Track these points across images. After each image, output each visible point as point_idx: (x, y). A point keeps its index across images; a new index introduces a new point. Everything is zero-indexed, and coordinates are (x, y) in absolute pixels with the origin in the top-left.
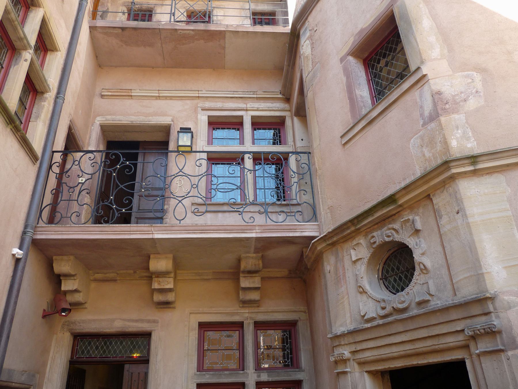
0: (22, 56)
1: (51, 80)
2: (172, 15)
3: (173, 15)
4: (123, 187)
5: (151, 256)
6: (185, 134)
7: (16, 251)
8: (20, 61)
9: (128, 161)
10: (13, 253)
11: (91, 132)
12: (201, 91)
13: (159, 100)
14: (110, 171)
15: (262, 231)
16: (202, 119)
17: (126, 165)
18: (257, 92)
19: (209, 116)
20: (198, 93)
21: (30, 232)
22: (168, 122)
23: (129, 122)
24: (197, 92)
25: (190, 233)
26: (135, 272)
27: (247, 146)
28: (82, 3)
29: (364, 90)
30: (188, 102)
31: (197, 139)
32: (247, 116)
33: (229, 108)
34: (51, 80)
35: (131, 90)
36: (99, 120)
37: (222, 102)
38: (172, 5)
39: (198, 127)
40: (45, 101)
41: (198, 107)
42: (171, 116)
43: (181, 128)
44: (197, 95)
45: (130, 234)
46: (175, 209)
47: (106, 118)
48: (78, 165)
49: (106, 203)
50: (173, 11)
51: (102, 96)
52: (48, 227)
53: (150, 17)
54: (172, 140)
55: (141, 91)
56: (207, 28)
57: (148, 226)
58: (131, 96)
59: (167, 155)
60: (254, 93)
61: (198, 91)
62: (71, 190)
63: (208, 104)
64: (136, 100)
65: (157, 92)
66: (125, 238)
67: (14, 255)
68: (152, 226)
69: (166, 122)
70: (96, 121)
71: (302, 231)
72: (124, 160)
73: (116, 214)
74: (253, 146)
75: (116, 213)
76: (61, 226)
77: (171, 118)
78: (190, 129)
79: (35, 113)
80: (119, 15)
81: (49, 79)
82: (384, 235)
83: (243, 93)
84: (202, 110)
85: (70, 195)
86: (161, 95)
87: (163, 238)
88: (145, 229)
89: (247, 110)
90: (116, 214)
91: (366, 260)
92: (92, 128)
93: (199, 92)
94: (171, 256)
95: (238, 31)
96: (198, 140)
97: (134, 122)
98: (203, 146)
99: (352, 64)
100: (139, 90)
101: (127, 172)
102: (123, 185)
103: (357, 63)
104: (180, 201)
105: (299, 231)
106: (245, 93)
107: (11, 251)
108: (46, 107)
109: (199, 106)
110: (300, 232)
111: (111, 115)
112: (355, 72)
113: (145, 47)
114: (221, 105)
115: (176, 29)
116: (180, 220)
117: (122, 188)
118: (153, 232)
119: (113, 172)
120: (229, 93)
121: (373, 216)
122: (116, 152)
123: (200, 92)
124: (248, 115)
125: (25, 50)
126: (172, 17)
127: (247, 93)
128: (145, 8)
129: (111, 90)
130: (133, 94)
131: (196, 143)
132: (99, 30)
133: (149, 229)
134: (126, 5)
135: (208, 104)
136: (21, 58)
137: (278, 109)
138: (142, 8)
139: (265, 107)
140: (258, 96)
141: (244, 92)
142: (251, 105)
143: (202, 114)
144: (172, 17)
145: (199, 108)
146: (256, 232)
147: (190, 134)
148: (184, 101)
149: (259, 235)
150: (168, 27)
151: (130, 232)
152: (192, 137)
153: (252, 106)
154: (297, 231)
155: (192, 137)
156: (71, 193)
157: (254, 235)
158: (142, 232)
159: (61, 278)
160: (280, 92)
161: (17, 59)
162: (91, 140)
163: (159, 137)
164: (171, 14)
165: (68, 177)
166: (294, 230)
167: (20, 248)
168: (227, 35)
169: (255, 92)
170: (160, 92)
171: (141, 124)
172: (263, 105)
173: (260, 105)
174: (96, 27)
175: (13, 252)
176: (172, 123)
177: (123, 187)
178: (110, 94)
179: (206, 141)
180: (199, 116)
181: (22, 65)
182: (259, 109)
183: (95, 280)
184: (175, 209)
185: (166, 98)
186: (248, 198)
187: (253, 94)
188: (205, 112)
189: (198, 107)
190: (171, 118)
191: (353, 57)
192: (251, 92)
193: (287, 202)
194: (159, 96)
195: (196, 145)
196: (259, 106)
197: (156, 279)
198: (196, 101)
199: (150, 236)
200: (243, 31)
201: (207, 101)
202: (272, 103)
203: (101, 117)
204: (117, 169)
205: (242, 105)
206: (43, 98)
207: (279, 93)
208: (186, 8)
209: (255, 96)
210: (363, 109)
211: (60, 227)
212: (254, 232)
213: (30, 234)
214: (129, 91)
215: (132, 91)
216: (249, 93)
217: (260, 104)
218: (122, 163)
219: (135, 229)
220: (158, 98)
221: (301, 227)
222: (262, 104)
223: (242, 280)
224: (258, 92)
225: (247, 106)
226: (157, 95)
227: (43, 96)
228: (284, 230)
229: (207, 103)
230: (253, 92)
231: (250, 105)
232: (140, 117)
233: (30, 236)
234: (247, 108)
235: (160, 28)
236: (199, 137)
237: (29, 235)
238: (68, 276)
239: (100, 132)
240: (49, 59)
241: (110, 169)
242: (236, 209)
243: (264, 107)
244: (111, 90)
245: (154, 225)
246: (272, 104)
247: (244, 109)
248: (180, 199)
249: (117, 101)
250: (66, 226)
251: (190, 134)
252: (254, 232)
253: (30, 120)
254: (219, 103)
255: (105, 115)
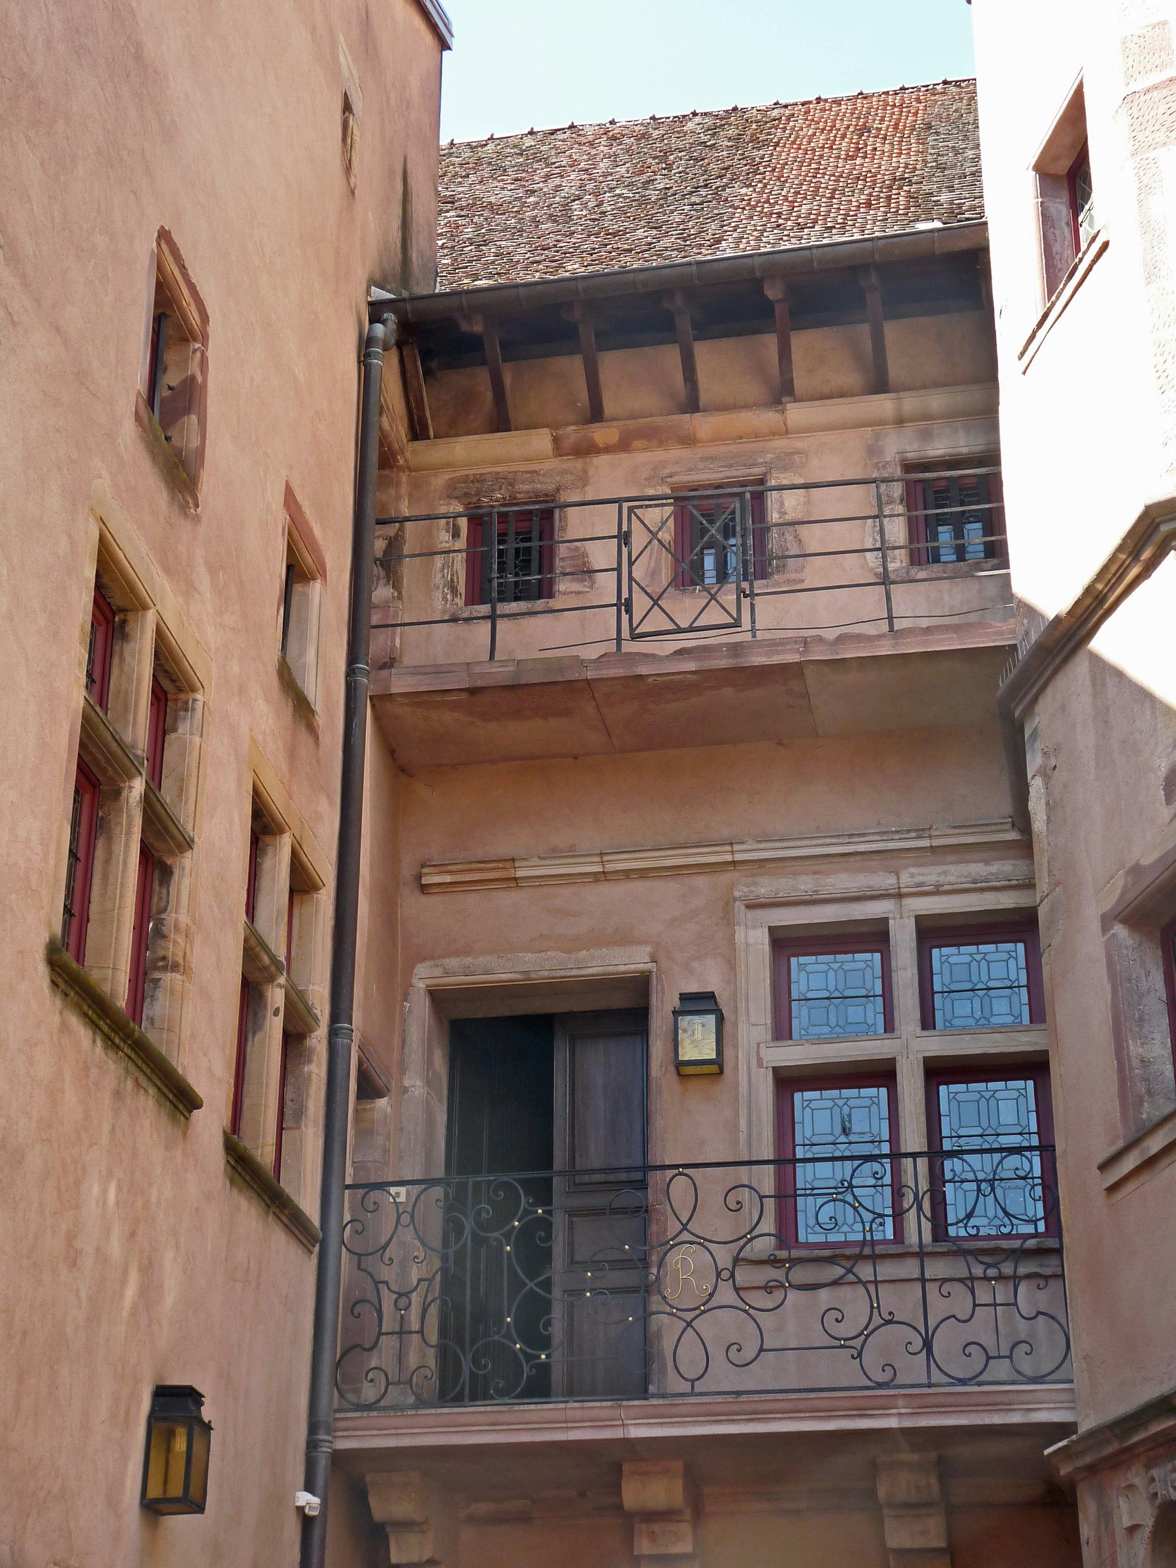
0: (266, 1003)
1: (316, 988)
2: (623, 607)
3: (627, 612)
4: (535, 1288)
5: (626, 1468)
6: (697, 1019)
7: (308, 1500)
8: (264, 1017)
9: (541, 1206)
10: (299, 1504)
11: (404, 1021)
12: (742, 843)
13: (604, 882)
14: (496, 1239)
15: (915, 1411)
16: (751, 940)
17: (537, 1218)
18: (930, 829)
19: (771, 930)
20: (732, 852)
21: (326, 1441)
22: (641, 967)
23: (519, 976)
24: (728, 848)
25: (722, 1421)
26: (582, 1494)
27: (904, 1037)
28: (355, 681)
29: (1153, 1039)
30: (700, 881)
31: (735, 1024)
32: (902, 917)
33: (839, 895)
34: (316, 988)
35: (513, 860)
36: (424, 976)
37: (815, 873)
38: (618, 569)
39: (738, 977)
40: (310, 1061)
41: (735, 900)
42: (647, 942)
43: (684, 997)
44: (729, 858)
45: (567, 1428)
46: (676, 1347)
47: (444, 968)
48: (409, 1225)
49: (496, 1338)
50: (625, 595)
51: (424, 889)
52: (361, 1417)
53: (548, 518)
54: (659, 1032)
55: (543, 862)
56: (740, 660)
57: (611, 1407)
58: (516, 879)
59: (645, 1040)
60: (920, 833)
61: (731, 844)
62: (403, 1302)
63: (765, 888)
64: (530, 890)
65: (597, 859)
66: (554, 1440)
67: (300, 1509)
68: (620, 1406)
69: (633, 967)
70: (415, 981)
71: (1028, 1410)
72: (529, 1204)
73: (526, 1369)
74: (926, 1033)
75: (525, 1365)
76: (392, 1414)
77: (648, 949)
78: (711, 996)
79: (292, 1101)
80: (441, 542)
81: (311, 987)
82: (1169, 1484)
83: (885, 838)
84: (748, 907)
85: (402, 1317)
86: (610, 867)
87: (651, 1438)
88: (603, 1414)
89: (900, 896)
90: (525, 1369)
91: (1146, 1533)
92: (404, 1006)
93: (734, 846)
94: (678, 1465)
95: (844, 659)
96: (740, 1026)
97: (533, 975)
98: (758, 1044)
99: (1124, 951)
100: (539, 857)
101: (541, 1242)
102: (535, 1282)
103: (1141, 944)
104: (689, 1324)
105: (1019, 1409)
106: (890, 837)
107: (294, 1499)
108: (314, 1076)
109: (737, 894)
110: (1022, 1412)
111: (458, 953)
112: (1129, 981)
113: (546, 719)
114: (809, 886)
115: (640, 675)
116: (693, 1381)
117: (531, 1288)
118: (625, 1422)
119: (504, 1241)
120: (834, 841)
121: (1146, 1428)
122: (506, 1179)
123: (736, 847)
124: (905, 914)
125: (270, 982)
126: (625, 617)
127: (897, 837)
128: (527, 496)
129: (450, 868)
130: (520, 873)
131: (735, 1037)
132: (400, 699)
133: (615, 1413)
134: (459, 493)
135: (765, 888)
136: (265, 1007)
137: (1007, 883)
138: (515, 498)
139: (963, 880)
140: (936, 842)
141: (885, 833)
142: (912, 876)
143: (749, 924)
144: (625, 617)
145: (737, 903)
146: (900, 1414)
147: (711, 1019)
148: (687, 880)
149: (909, 1423)
150: (615, 671)
151: (568, 1423)
152: (720, 1020)
153: (919, 879)
154: (1016, 1409)
155: (720, 1020)
156: (403, 1312)
157: (893, 1423)
158: (596, 1422)
159: (388, 1529)
160: (1013, 822)
161: (255, 1014)
162: (406, 1050)
163: (619, 1001)
164: (618, 605)
165: (389, 1263)
166: (1006, 1406)
167: (309, 1487)
168: (808, 671)
169: (923, 830)
170: (605, 858)
171: (554, 978)
172: (955, 872)
173: (945, 873)
174: (391, 694)
175: (298, 1501)
176: (651, 966)
177: (535, 1288)
178: (448, 879)
179: (765, 1024)
180: (740, 935)
181: (271, 1027)
182: (941, 889)
183: (472, 1520)
184: (676, 1347)
185: (627, 874)
186: (875, 1305)
187: (919, 837)
188: (759, 913)
189: (735, 900)
190: (648, 949)
191: (1129, 926)
192: (908, 831)
193: (1038, 1243)
194: (604, 872)
195: (736, 1046)
196: (942, 879)
197: (644, 1526)
198: (725, 878)
199: (618, 1434)
200: (859, 657)
201: (761, 875)
202: (987, 862)
203: (428, 963)
204: (515, 1232)
205: (885, 881)
206: (303, 1054)
207: (1008, 827)
208: (669, 480)
209: (925, 843)
210: (1145, 1104)
211: (392, 1416)
212: (894, 1415)
213: (326, 1447)
214: (508, 865)
215: (517, 864)
216: (903, 836)
217: (945, 868)
218: (526, 1212)
219: (579, 1414)
220: (603, 877)
221: (1025, 1398)
222: (952, 868)
223: (889, 1524)
224: (936, 829)
225: (898, 879)
226: (597, 868)
227: (302, 1043)
228: (976, 1406)
229: (763, 880)
230: (915, 831)
231: (908, 878)
232: (549, 953)
233: (326, 1452)
234: (899, 888)
235: (589, 678)
236: (742, 1017)
237: (324, 1449)
238: (405, 1525)
239: (429, 1017)
240: (300, 920)
241: (496, 1234)
242: (842, 1342)
243: (959, 880)
244: (450, 868)
245: (625, 1403)
246: (986, 865)
247: (889, 892)
248: (689, 1316)
249: (472, 898)
250: (405, 1413)
251: (711, 1019)
252: (894, 1415)
253: (284, 1126)
254: (804, 877)
255: (439, 957)
